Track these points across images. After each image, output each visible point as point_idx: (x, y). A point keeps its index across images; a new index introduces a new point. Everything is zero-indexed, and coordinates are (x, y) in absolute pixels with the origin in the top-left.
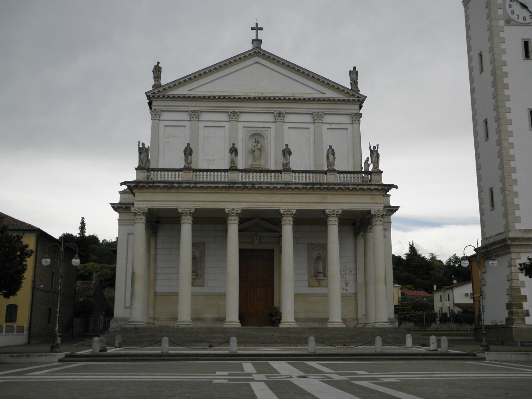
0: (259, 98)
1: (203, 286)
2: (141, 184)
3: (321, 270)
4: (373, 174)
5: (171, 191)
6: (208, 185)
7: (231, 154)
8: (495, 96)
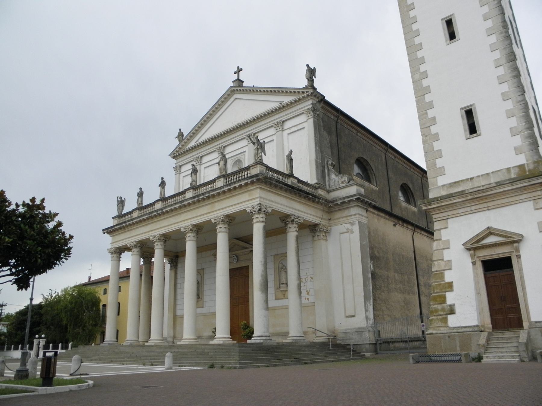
1: (203, 307)
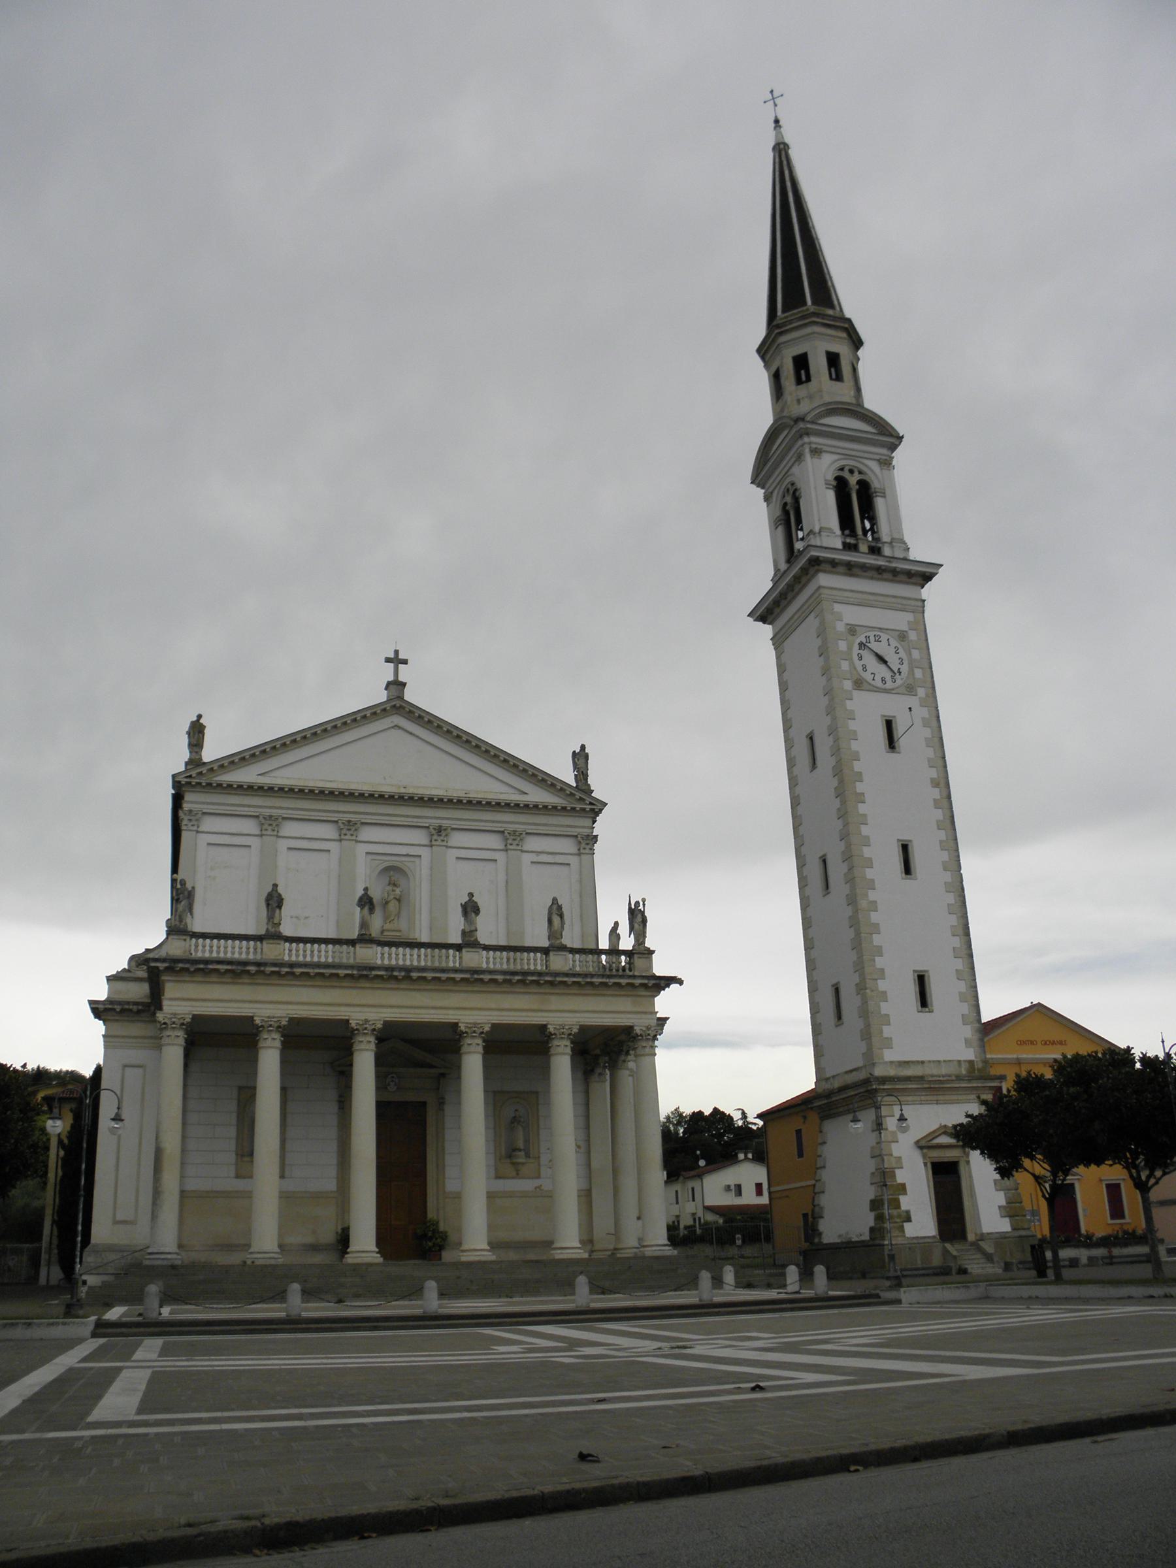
0: (401, 797)
2: (181, 965)
3: (521, 1144)
4: (636, 956)
5: (241, 981)
6: (317, 971)
7: (362, 909)
8: (843, 814)
